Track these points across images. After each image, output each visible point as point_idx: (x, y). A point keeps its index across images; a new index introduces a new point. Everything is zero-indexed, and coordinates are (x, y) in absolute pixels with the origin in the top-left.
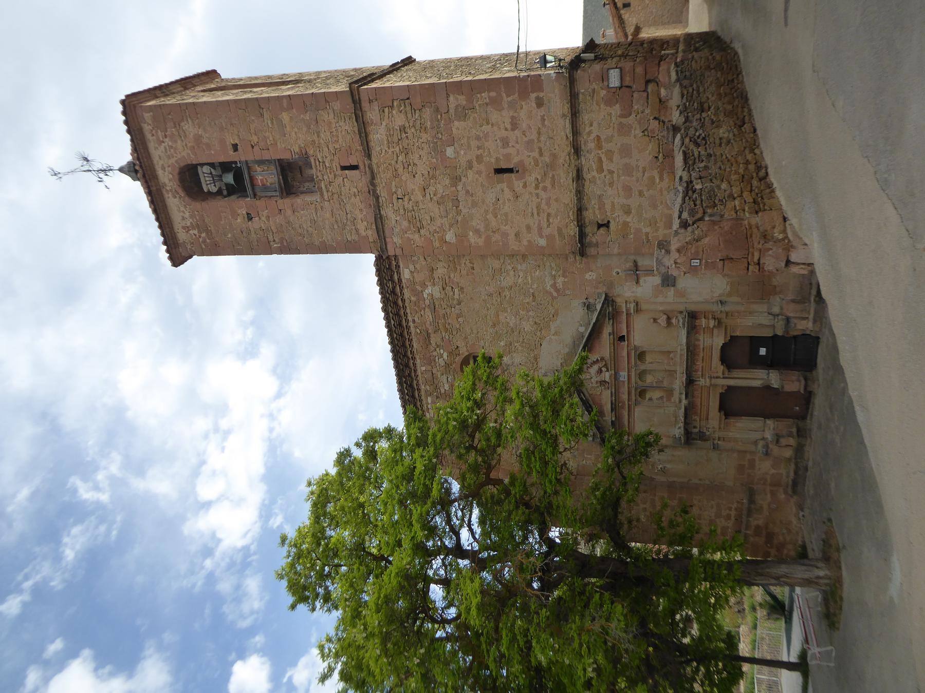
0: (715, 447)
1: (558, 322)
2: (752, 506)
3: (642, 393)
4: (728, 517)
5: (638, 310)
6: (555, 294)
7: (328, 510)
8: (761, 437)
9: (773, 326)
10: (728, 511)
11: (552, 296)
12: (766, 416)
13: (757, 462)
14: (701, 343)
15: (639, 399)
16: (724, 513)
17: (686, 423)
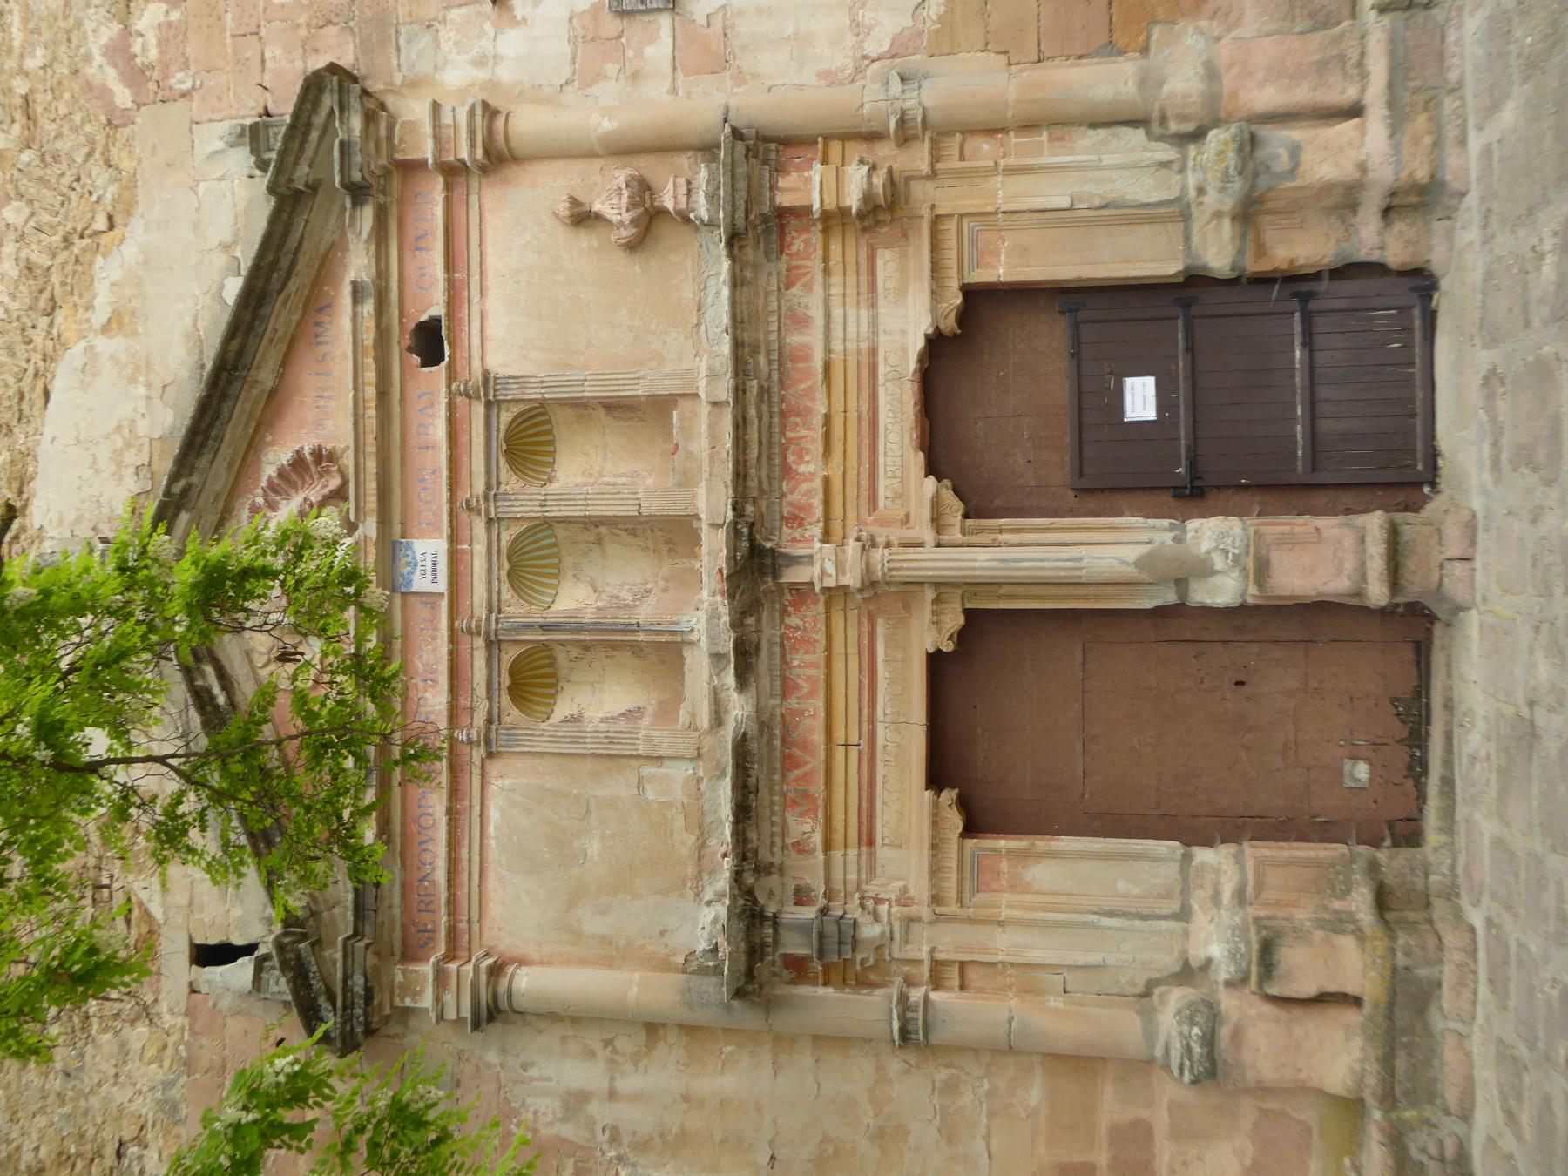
0: (913, 1035)
1: (130, 251)
3: (532, 677)
5: (498, 158)
6: (123, 97)
8: (1168, 962)
9: (1179, 212)
11: (110, 107)
12: (1193, 830)
14: (813, 339)
15: (512, 714)
17: (743, 850)
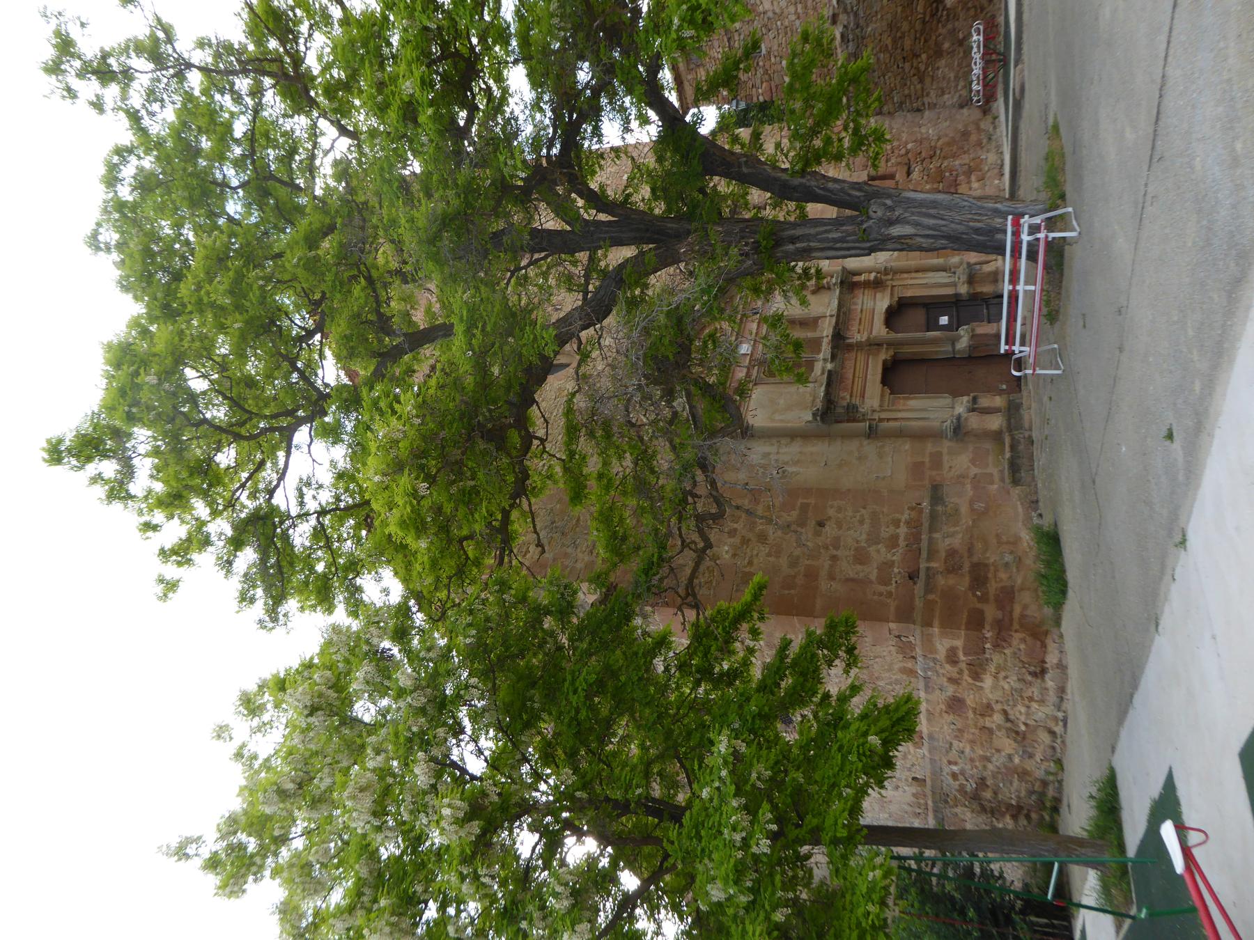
0: (872, 433)
2: (939, 508)
4: (893, 542)
7: (339, 453)
10: (891, 529)
13: (945, 458)
16: (886, 532)
